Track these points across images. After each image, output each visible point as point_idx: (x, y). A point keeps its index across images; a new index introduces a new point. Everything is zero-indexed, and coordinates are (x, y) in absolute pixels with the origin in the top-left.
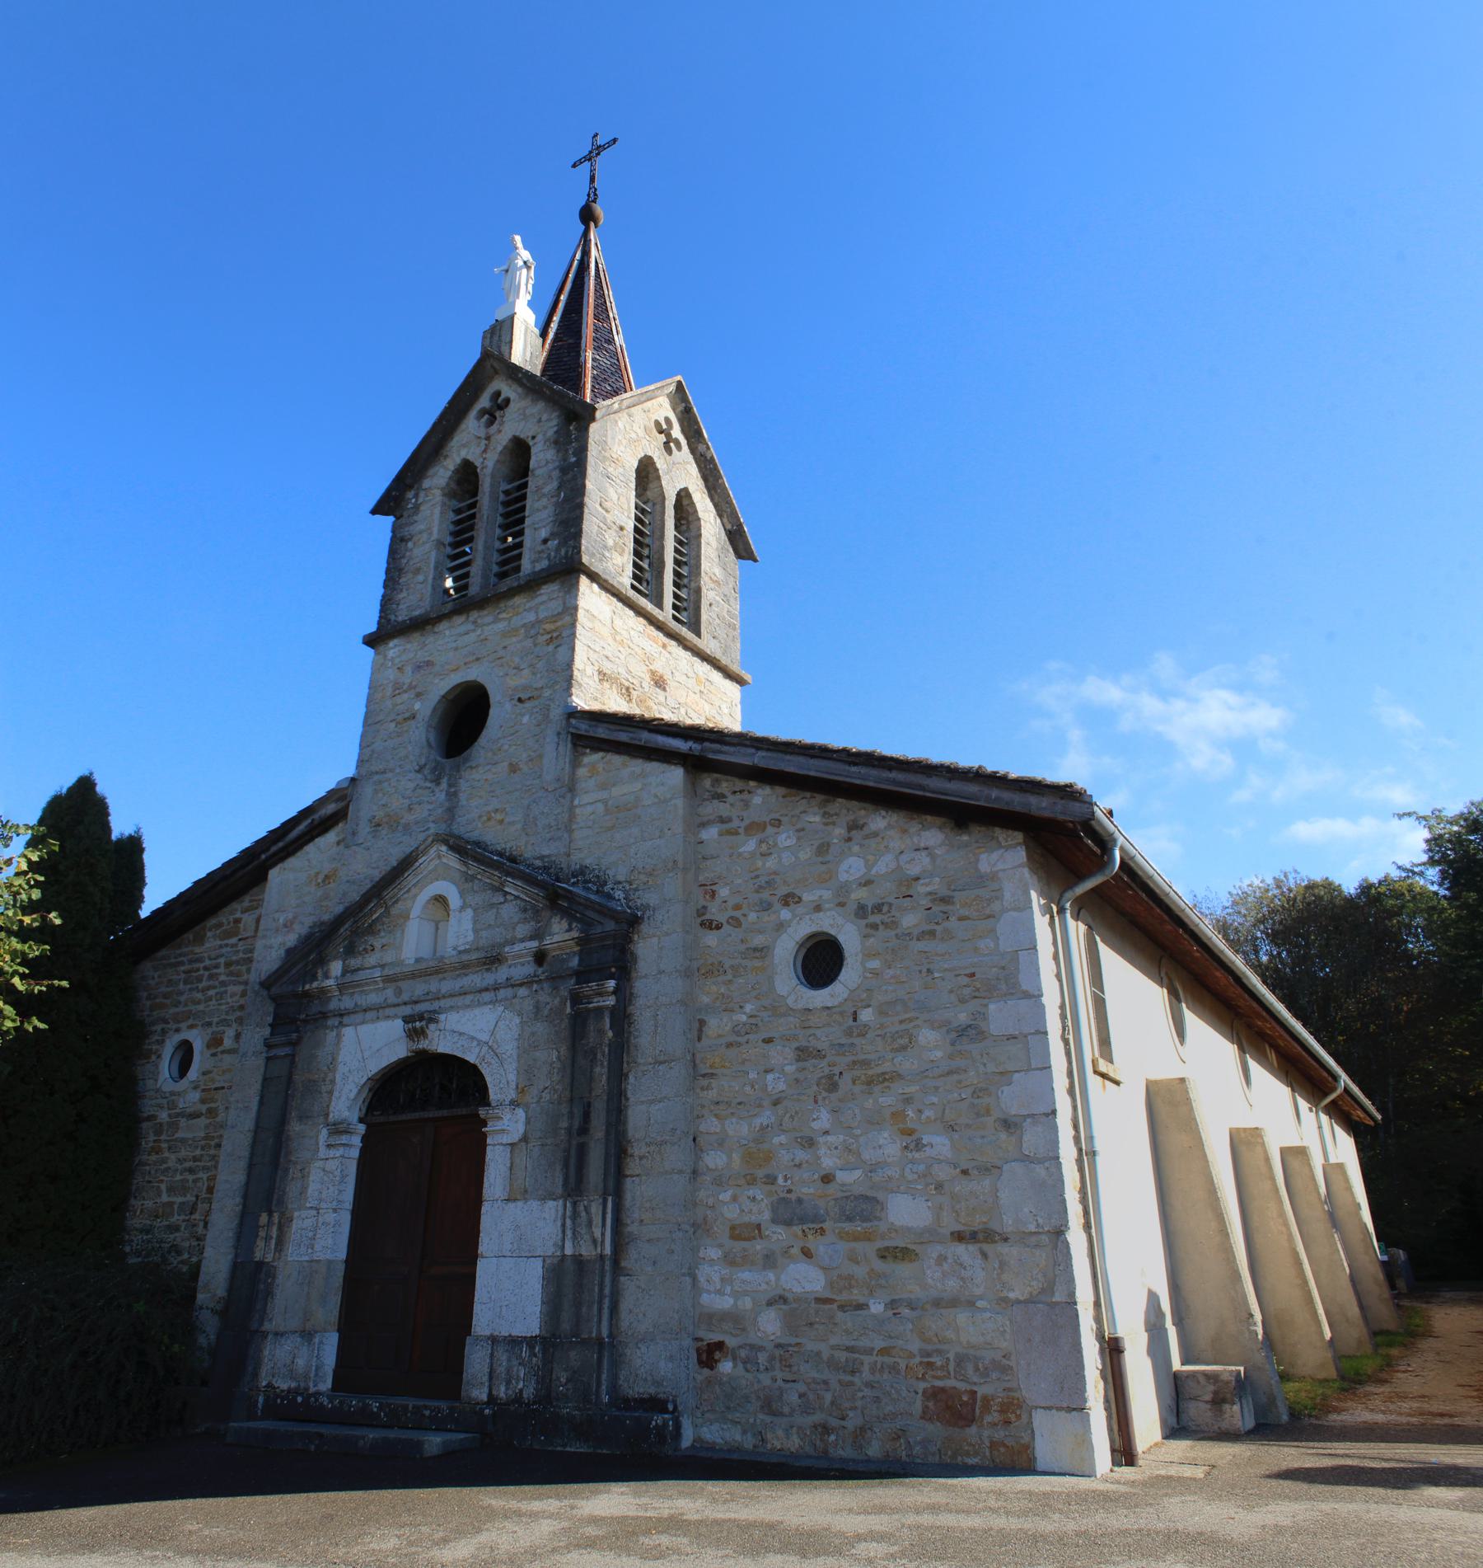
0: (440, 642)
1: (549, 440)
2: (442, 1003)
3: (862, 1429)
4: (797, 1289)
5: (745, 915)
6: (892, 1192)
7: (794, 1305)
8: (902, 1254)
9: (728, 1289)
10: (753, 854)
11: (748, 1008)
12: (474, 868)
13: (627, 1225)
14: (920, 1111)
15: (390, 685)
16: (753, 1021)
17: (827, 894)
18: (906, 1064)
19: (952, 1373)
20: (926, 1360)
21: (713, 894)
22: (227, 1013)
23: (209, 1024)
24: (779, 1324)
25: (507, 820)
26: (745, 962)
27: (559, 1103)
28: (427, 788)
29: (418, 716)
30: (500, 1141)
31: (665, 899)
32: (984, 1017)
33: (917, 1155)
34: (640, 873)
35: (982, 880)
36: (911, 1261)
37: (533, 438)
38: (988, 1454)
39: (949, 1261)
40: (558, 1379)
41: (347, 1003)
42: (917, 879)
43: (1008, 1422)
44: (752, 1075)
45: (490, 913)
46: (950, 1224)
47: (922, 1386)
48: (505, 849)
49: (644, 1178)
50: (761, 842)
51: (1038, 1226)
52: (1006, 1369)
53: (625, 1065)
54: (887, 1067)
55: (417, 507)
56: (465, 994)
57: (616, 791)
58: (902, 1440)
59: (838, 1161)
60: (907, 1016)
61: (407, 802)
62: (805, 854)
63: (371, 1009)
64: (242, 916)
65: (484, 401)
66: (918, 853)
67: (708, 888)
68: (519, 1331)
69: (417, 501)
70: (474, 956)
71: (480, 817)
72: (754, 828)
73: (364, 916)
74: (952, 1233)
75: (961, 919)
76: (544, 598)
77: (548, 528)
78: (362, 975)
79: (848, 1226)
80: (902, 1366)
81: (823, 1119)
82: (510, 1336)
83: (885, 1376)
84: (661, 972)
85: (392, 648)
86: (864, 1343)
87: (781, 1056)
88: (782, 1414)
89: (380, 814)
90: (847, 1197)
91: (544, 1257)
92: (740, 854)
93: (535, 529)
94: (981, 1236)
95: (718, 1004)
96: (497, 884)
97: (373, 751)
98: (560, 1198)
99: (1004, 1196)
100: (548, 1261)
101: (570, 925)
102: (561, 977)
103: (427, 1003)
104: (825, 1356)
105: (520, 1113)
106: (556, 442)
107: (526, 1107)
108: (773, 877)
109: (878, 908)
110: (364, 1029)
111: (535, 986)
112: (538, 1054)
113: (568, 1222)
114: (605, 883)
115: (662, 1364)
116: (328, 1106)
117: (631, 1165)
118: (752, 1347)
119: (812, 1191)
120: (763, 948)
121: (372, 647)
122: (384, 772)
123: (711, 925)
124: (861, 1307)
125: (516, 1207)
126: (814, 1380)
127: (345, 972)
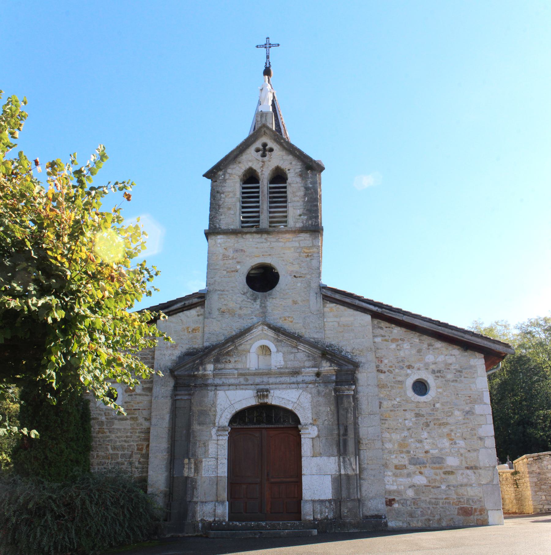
1: (296, 173)
2: (271, 386)
3: (440, 519)
4: (418, 483)
6: (447, 456)
8: (452, 473)
11: (398, 400)
12: (282, 337)
16: (400, 404)
17: (422, 365)
18: (451, 420)
21: (382, 361)
25: (294, 321)
26: (395, 385)
27: (332, 425)
28: (249, 302)
32: (474, 408)
33: (455, 446)
35: (471, 367)
37: (289, 170)
40: (344, 511)
41: (217, 381)
42: (451, 364)
44: (400, 421)
46: (464, 465)
47: (458, 507)
49: (368, 450)
52: (480, 501)
53: (357, 414)
54: (445, 421)
55: (225, 180)
56: (283, 384)
62: (414, 352)
63: (233, 385)
65: (258, 144)
68: (323, 498)
69: (225, 177)
70: (287, 371)
71: (280, 318)
74: (465, 467)
77: (302, 210)
78: (224, 371)
79: (434, 466)
80: (452, 502)
86: (440, 497)
87: (410, 415)
88: (416, 517)
89: (224, 308)
94: (474, 468)
95: (386, 397)
97: (215, 281)
100: (333, 476)
101: (331, 364)
103: (263, 386)
104: (428, 500)
105: (315, 428)
106: (301, 175)
107: (318, 426)
108: (403, 359)
109: (439, 371)
110: (228, 393)
111: (317, 385)
112: (321, 408)
113: (342, 464)
114: (342, 352)
115: (379, 505)
116: (214, 421)
117: (362, 446)
118: (405, 499)
119: (422, 455)
122: (224, 291)
123: (381, 372)
124: (439, 487)
126: (425, 508)
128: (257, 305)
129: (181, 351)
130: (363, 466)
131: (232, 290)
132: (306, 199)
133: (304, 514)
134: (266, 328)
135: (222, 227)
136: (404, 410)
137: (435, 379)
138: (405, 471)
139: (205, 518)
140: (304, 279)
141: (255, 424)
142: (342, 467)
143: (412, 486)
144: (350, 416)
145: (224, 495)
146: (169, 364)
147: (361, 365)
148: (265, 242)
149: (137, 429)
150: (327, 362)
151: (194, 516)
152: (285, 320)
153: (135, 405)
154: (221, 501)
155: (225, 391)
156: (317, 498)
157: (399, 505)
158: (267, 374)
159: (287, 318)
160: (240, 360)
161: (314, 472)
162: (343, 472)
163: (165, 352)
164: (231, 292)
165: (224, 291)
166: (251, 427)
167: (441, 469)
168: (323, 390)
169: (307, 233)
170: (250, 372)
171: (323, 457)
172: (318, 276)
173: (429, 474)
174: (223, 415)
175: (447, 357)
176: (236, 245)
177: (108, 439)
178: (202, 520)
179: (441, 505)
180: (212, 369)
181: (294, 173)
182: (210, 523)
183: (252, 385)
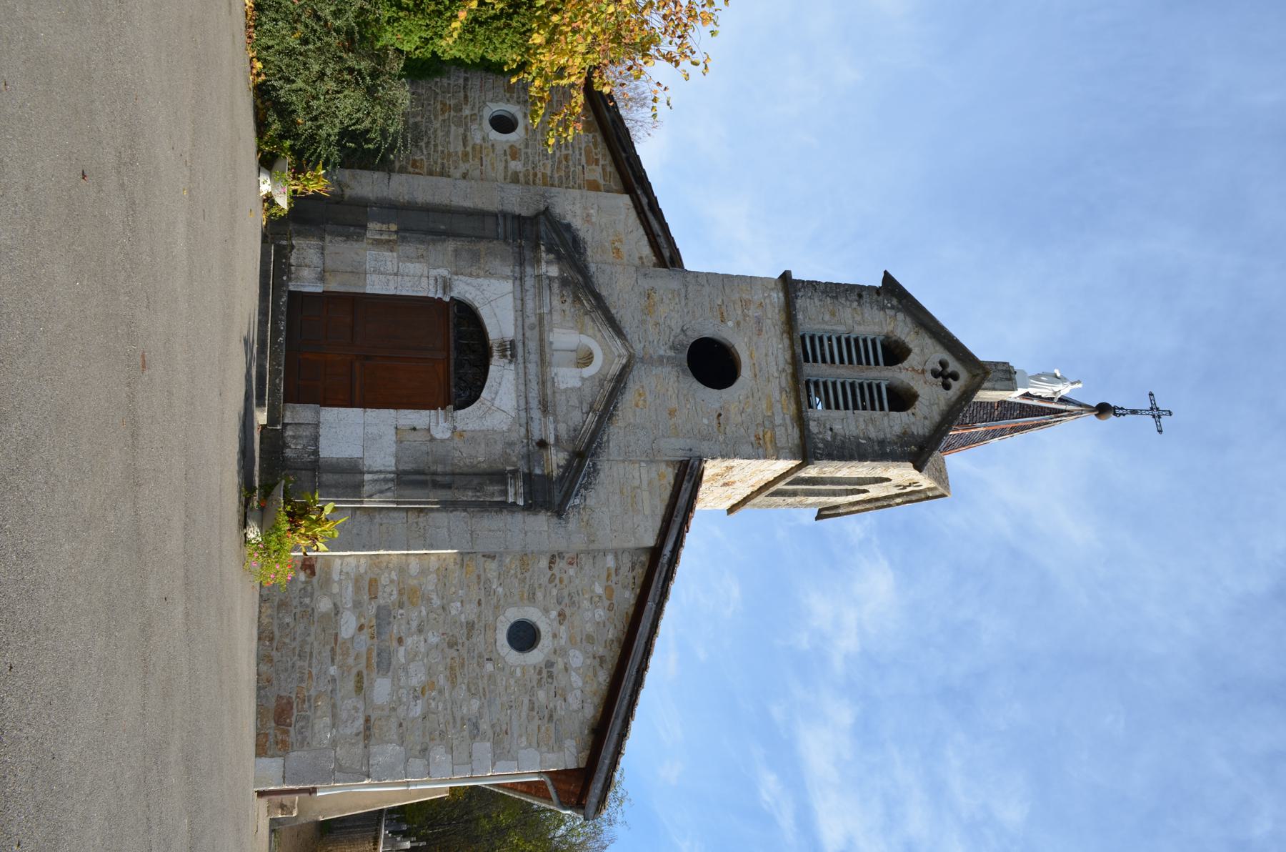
0: (775, 340)
2: (521, 366)
4: (342, 622)
5: (556, 586)
7: (334, 620)
8: (359, 688)
9: (342, 577)
10: (593, 591)
11: (500, 590)
12: (608, 386)
13: (380, 515)
14: (434, 699)
15: (750, 297)
17: (563, 642)
18: (462, 692)
19: (300, 714)
20: (306, 698)
21: (571, 564)
22: (533, 162)
23: (527, 146)
24: (324, 611)
26: (527, 586)
27: (452, 464)
29: (723, 325)
30: (432, 421)
31: (570, 535)
33: (411, 696)
34: (589, 515)
35: (560, 741)
36: (356, 691)
38: (262, 732)
39: (356, 714)
41: (529, 282)
42: (565, 700)
43: (277, 743)
45: (576, 401)
47: (294, 697)
48: (617, 411)
50: (600, 597)
51: (372, 765)
53: (472, 509)
54: (459, 680)
55: (883, 308)
56: (526, 385)
57: (646, 495)
58: (267, 683)
59: (410, 647)
60: (487, 693)
61: (661, 321)
62: (589, 628)
63: (523, 305)
64: (600, 166)
65: (954, 366)
66: (581, 702)
67: (575, 560)
68: (323, 442)
69: (889, 308)
70: (549, 392)
72: (609, 590)
73: (586, 295)
74: (369, 716)
75: (539, 727)
76: (790, 430)
77: (841, 432)
79: (375, 654)
80: (303, 685)
81: (433, 639)
82: (320, 436)
83: (298, 675)
84: (526, 533)
85: (778, 295)
87: (470, 612)
88: (278, 613)
89: (656, 297)
90: (390, 654)
91: (363, 458)
92: (594, 583)
93: (843, 419)
94: (368, 733)
96: (595, 406)
97: (703, 286)
98: (397, 468)
99: (390, 747)
100: (361, 461)
102: (529, 461)
105: (448, 435)
106: (905, 433)
107: (451, 439)
109: (550, 676)
110: (510, 298)
111: (525, 441)
112: (483, 446)
113: (382, 476)
114: (586, 489)
116: (462, 274)
119: (395, 631)
120: (534, 599)
121: (781, 277)
123: (552, 562)
125: (392, 435)
127: (550, 279)
128: (663, 351)
129: (580, 230)
130: (377, 516)
131: (688, 312)
132: (863, 441)
133: (294, 408)
134: (624, 361)
135: (799, 301)
136: (480, 600)
137: (535, 667)
138: (365, 597)
139: (295, 250)
140: (715, 430)
141: (456, 341)
142: (376, 477)
143: (337, 610)
144: (469, 496)
145: (334, 286)
146: (557, 210)
147: (563, 522)
148: (778, 370)
149: (448, 161)
150: (566, 460)
151: (300, 234)
152: (640, 395)
153: (489, 159)
154: (323, 276)
155: (513, 292)
156: (321, 431)
157: (303, 583)
158: (542, 360)
159: (642, 398)
160: (568, 319)
161: (370, 430)
162: (367, 477)
163: (579, 205)
164: (686, 310)
165: (686, 297)
166: (451, 334)
167: (367, 667)
168: (516, 452)
169: (800, 437)
170: (546, 333)
171: (394, 445)
172: (724, 453)
173: (358, 643)
174: (471, 288)
175: (578, 693)
176: (769, 321)
177: (432, 117)
178: (293, 247)
179: (299, 663)
180: (549, 274)
181: (908, 422)
182: (288, 258)
183: (524, 335)
